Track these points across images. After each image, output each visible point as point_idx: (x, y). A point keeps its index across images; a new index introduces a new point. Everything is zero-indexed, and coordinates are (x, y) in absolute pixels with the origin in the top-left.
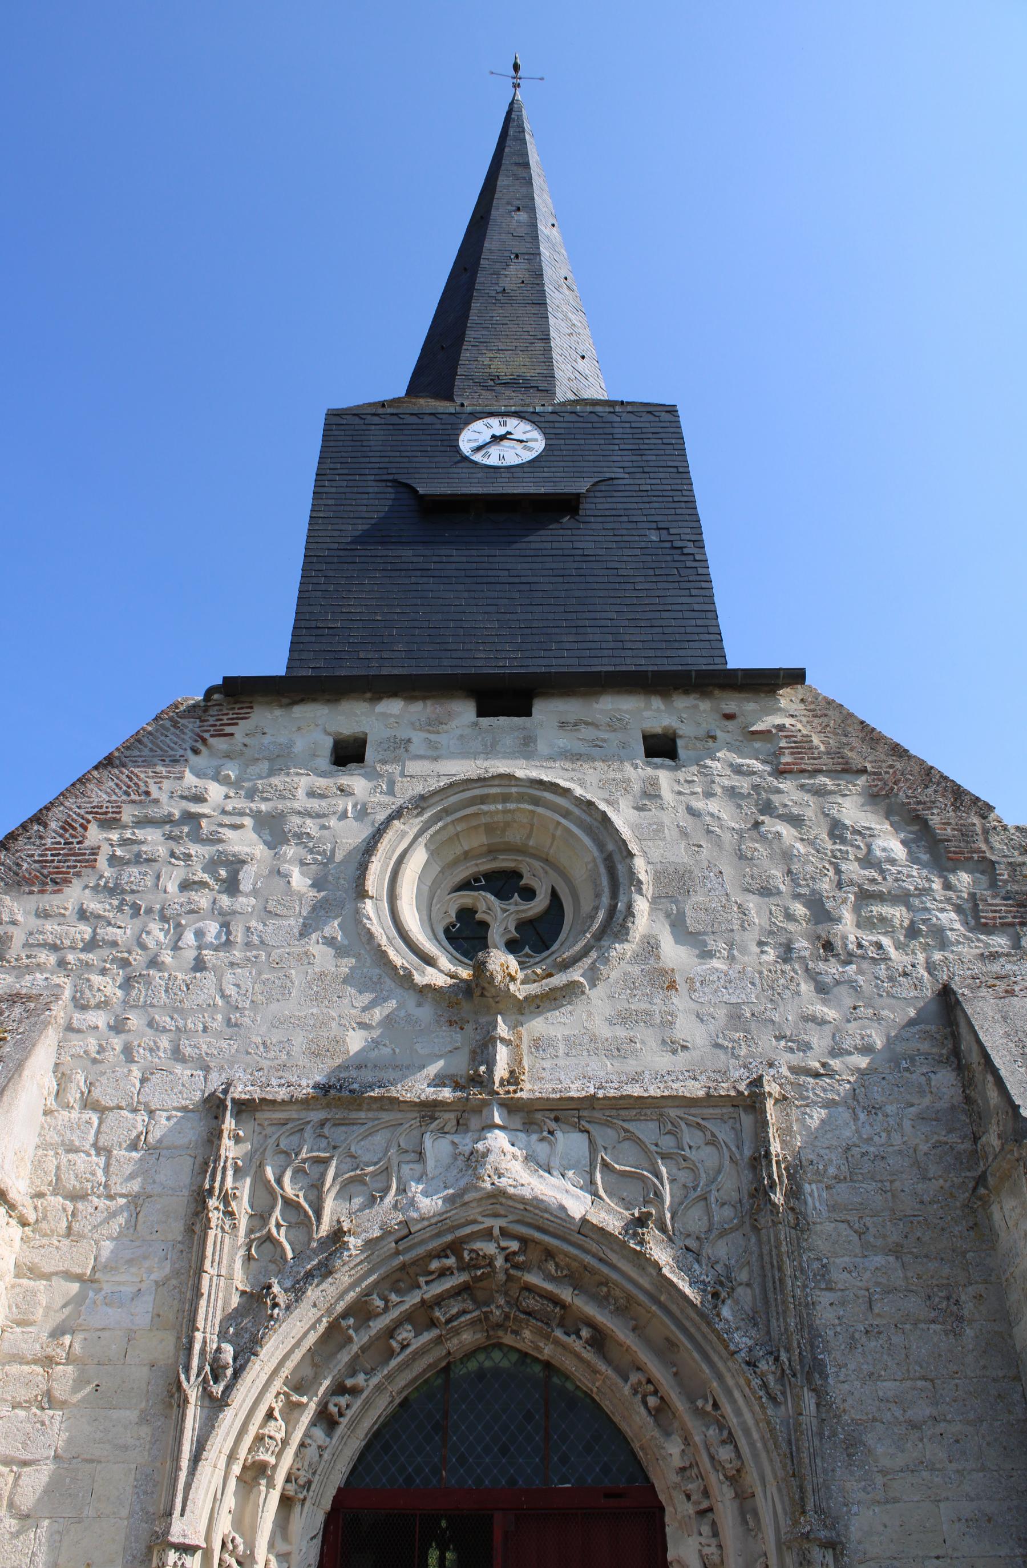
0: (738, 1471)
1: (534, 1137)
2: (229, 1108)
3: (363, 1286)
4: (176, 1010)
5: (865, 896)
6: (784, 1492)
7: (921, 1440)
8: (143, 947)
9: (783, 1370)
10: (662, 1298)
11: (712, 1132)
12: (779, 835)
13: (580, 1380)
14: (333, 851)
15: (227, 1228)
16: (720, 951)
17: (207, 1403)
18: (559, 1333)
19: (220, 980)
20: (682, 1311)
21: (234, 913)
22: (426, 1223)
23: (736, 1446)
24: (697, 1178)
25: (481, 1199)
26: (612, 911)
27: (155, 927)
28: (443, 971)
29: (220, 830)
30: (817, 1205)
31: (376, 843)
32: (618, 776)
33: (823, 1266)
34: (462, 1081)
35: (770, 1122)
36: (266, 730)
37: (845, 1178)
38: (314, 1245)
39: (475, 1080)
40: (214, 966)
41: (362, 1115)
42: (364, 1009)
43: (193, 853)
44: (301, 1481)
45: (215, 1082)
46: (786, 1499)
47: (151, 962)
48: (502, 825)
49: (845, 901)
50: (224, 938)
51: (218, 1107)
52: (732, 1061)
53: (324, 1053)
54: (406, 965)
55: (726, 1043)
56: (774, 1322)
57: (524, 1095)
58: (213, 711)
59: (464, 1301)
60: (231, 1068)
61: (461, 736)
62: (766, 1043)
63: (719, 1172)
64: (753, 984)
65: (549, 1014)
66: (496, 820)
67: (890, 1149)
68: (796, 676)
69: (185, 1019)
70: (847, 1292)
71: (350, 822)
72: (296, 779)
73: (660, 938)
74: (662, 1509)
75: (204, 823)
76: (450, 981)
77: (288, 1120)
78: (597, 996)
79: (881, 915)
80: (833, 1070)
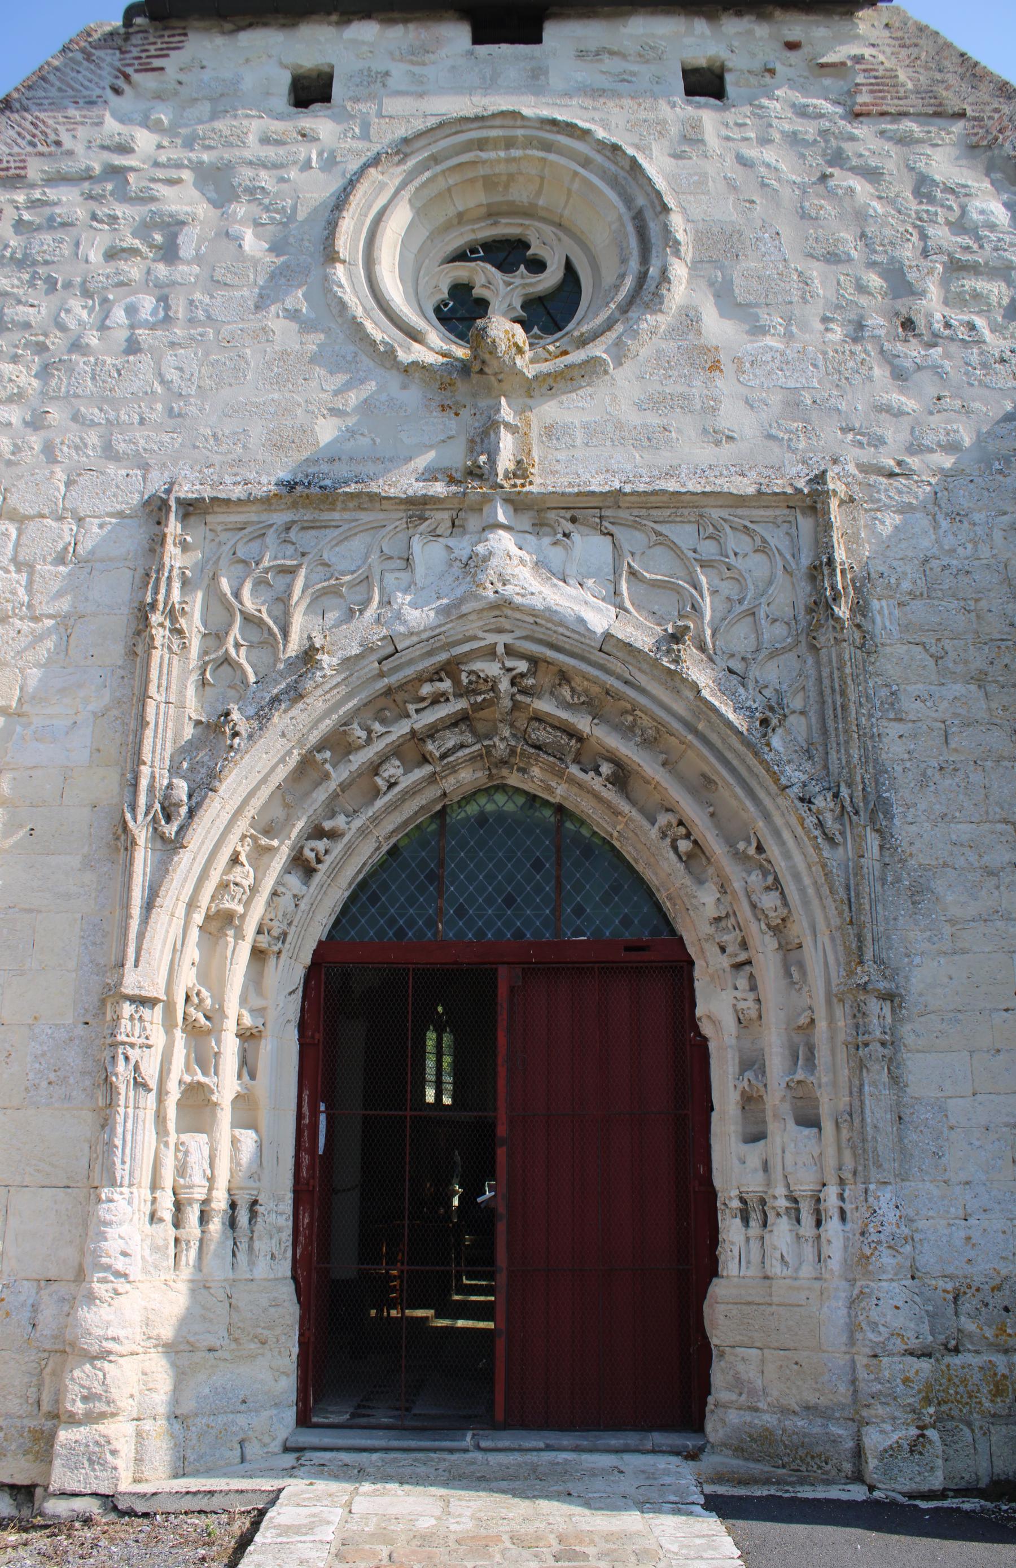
0: (783, 920)
1: (547, 541)
2: (173, 509)
3: (344, 709)
4: (103, 400)
5: (956, 267)
6: (839, 942)
7: (998, 887)
8: (62, 328)
9: (843, 807)
10: (700, 727)
11: (762, 537)
12: (851, 190)
13: (598, 824)
14: (294, 208)
15: (175, 648)
16: (774, 327)
17: (159, 845)
18: (574, 770)
19: (158, 364)
20: (724, 740)
21: (173, 284)
22: (415, 639)
23: (782, 893)
24: (743, 588)
25: (482, 610)
28: (435, 347)
29: (152, 186)
30: (887, 624)
31: (347, 196)
32: (652, 116)
33: (892, 694)
34: (458, 476)
35: (835, 525)
36: (204, 63)
37: (922, 594)
38: (281, 666)
40: (150, 346)
41: (336, 515)
42: (336, 393)
43: (119, 214)
44: (275, 933)
45: (156, 484)
46: (840, 948)
47: (73, 345)
48: (504, 178)
49: (931, 272)
50: (162, 314)
51: (160, 509)
52: (788, 455)
53: (287, 444)
54: (387, 339)
55: (781, 435)
56: (833, 755)
57: (534, 488)
58: (137, 39)
59: (462, 733)
60: (175, 465)
61: (453, 67)
63: (770, 583)
64: (815, 366)
65: (564, 398)
66: (497, 171)
67: (976, 563)
69: (117, 411)
70: (920, 724)
71: (316, 174)
72: (245, 122)
73: (701, 309)
74: (691, 963)
75: (131, 177)
76: (441, 360)
77: (245, 523)
79: (975, 290)
80: (911, 470)
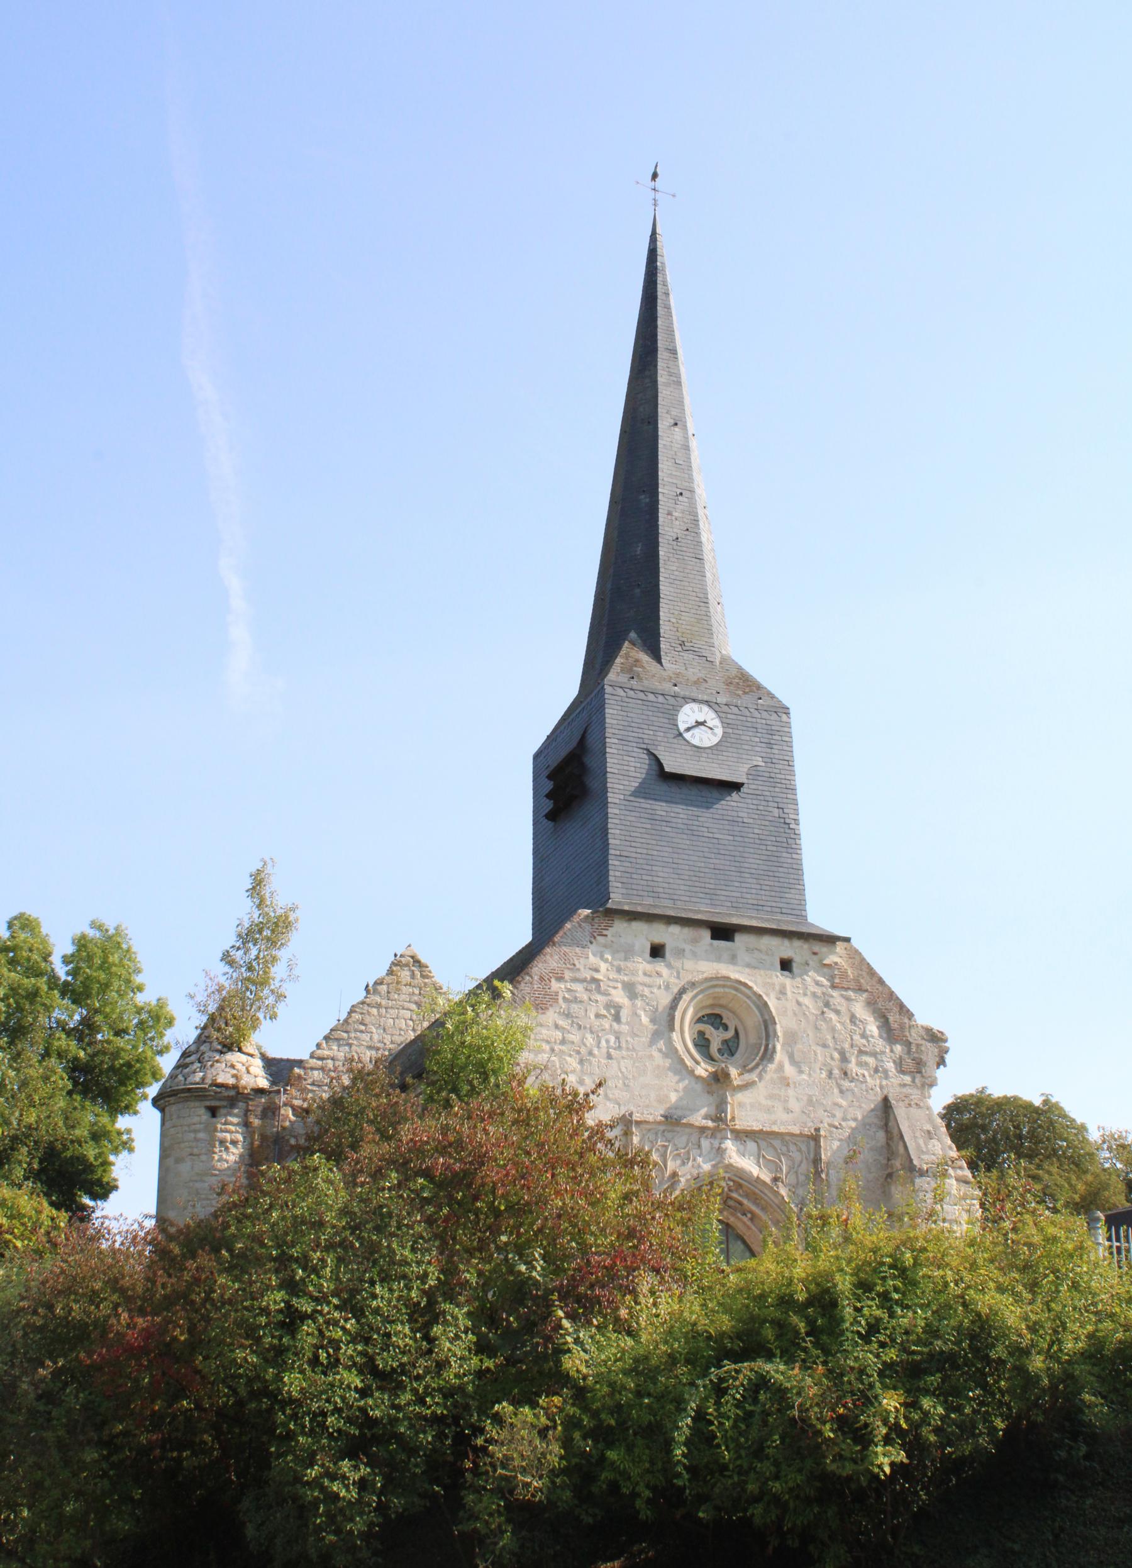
5: (861, 1052)
8: (585, 1045)
26: (767, 1046)
27: (588, 1036)
39: (719, 1117)
62: (821, 1113)
68: (847, 940)
78: (760, 1085)
